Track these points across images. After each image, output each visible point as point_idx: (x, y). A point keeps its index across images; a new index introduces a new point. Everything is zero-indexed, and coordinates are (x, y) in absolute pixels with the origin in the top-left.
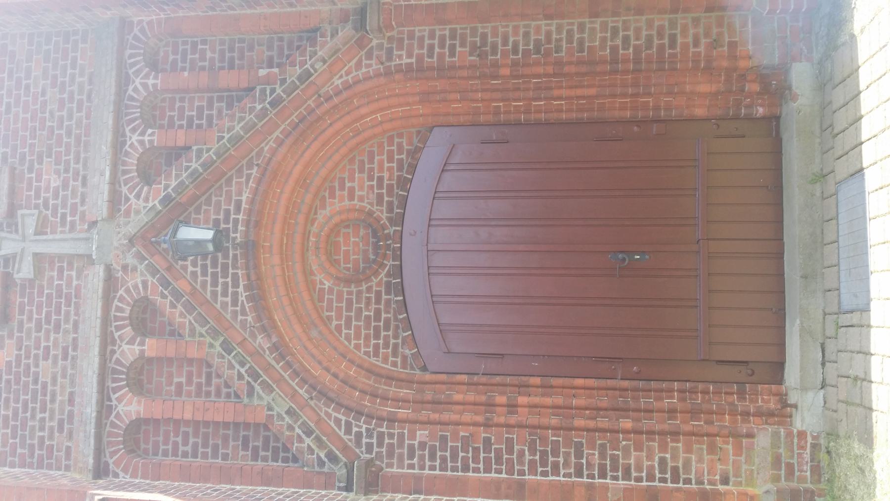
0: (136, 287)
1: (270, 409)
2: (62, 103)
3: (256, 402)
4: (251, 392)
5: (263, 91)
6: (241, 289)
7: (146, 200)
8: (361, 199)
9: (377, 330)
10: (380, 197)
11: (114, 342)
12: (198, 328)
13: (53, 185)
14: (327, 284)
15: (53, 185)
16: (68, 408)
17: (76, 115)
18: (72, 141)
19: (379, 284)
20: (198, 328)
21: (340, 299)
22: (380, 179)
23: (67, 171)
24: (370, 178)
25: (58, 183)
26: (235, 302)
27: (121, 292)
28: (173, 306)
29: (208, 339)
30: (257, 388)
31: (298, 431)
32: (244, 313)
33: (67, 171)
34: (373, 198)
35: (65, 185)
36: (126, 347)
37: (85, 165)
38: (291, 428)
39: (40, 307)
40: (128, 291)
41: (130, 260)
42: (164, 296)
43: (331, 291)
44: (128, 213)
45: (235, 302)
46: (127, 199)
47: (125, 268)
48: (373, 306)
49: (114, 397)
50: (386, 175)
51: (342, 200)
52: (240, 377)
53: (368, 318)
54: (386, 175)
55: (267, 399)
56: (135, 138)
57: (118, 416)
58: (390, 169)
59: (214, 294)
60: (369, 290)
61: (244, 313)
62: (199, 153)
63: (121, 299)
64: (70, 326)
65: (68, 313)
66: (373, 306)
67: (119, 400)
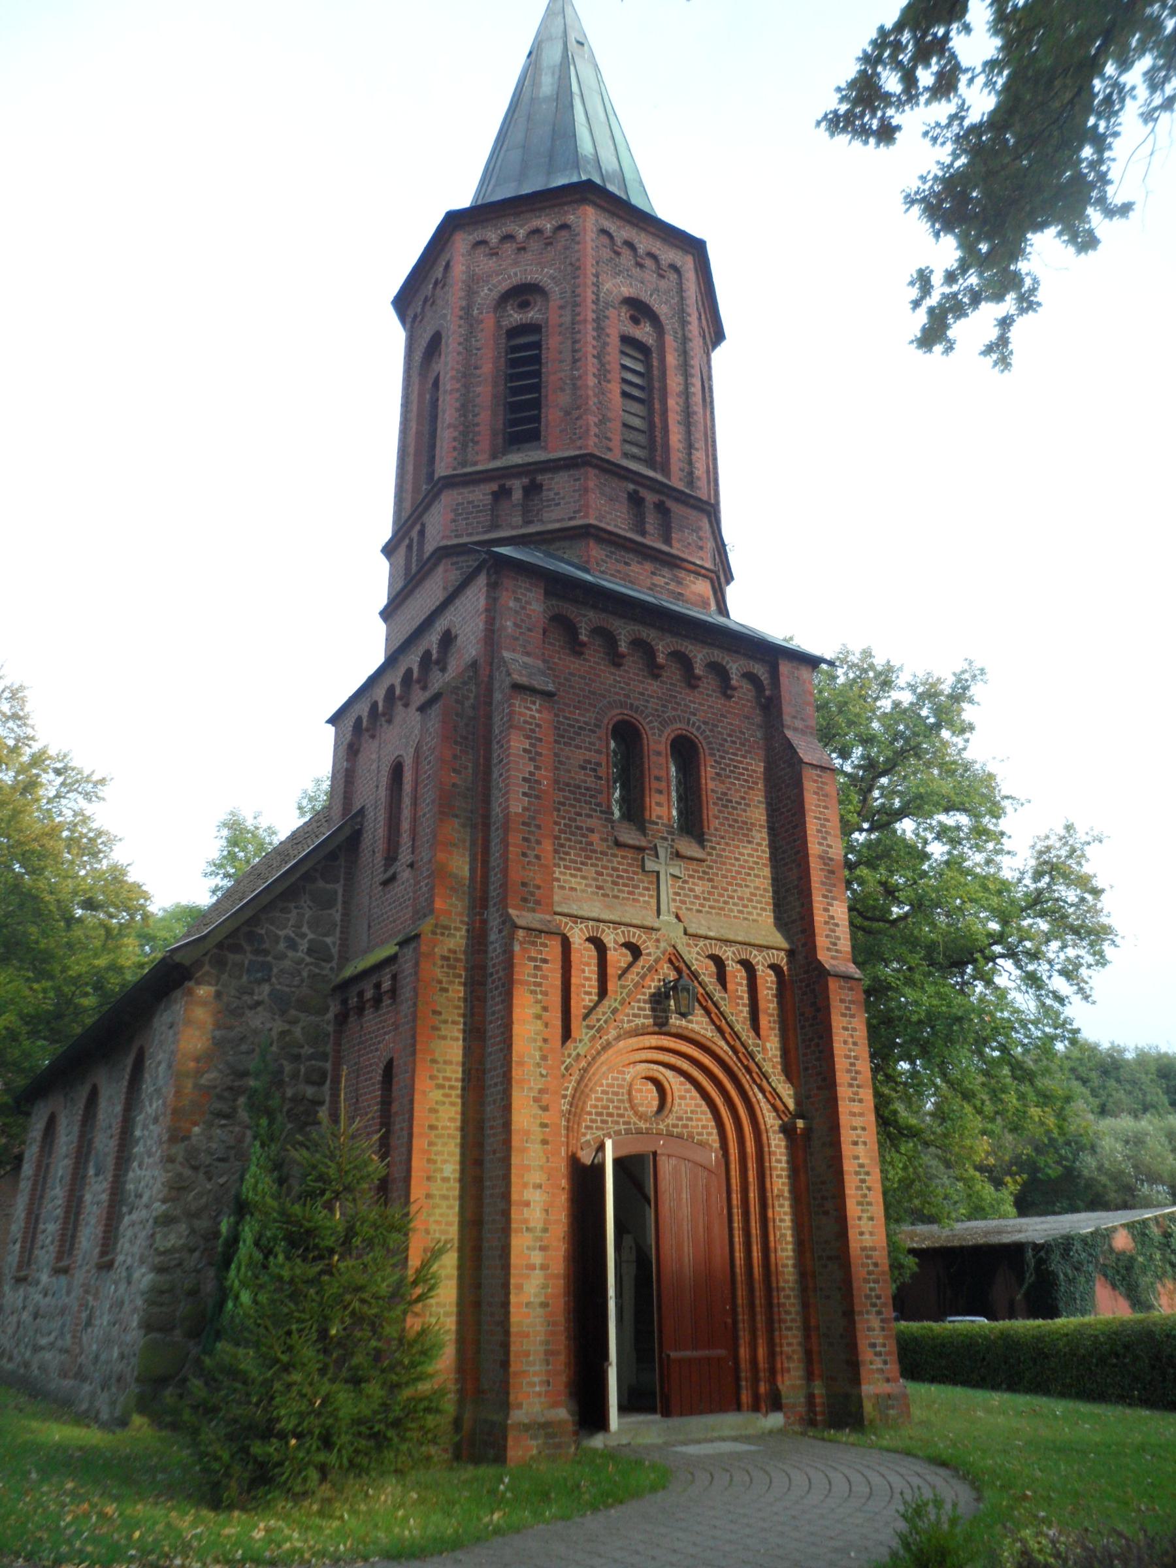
0: (647, 948)
1: (581, 1041)
2: (741, 899)
3: (584, 1031)
4: (590, 1027)
5: (758, 1046)
6: (642, 1020)
7: (697, 960)
8: (680, 1105)
9: (600, 1114)
10: (680, 1119)
11: (615, 929)
12: (626, 991)
13: (696, 888)
14: (628, 1077)
15: (696, 888)
16: (567, 886)
17: (735, 908)
18: (721, 905)
19: (629, 1117)
20: (626, 991)
21: (620, 1086)
22: (690, 1119)
23: (705, 899)
24: (692, 1112)
25: (698, 893)
26: (635, 1015)
27: (644, 937)
28: (638, 974)
29: (619, 998)
30: (592, 1032)
31: (568, 1061)
32: (629, 1021)
33: (705, 899)
34: (680, 1113)
35: (696, 897)
36: (612, 936)
37: (708, 912)
38: (569, 1056)
39: (626, 871)
40: (645, 942)
41: (663, 945)
42: (643, 967)
43: (624, 1079)
44: (688, 945)
45: (635, 1015)
46: (696, 946)
47: (658, 941)
48: (615, 1112)
49: (583, 926)
50: (694, 1123)
51: (679, 1090)
52: (598, 1020)
53: (608, 1108)
54: (694, 1123)
55: (586, 1039)
56: (730, 954)
57: (572, 928)
58: (697, 1127)
59: (639, 1001)
60: (625, 1109)
61: (629, 1021)
62: (723, 999)
63: (640, 937)
64: (616, 893)
65: (623, 891)
66: (615, 1112)
67: (581, 930)
